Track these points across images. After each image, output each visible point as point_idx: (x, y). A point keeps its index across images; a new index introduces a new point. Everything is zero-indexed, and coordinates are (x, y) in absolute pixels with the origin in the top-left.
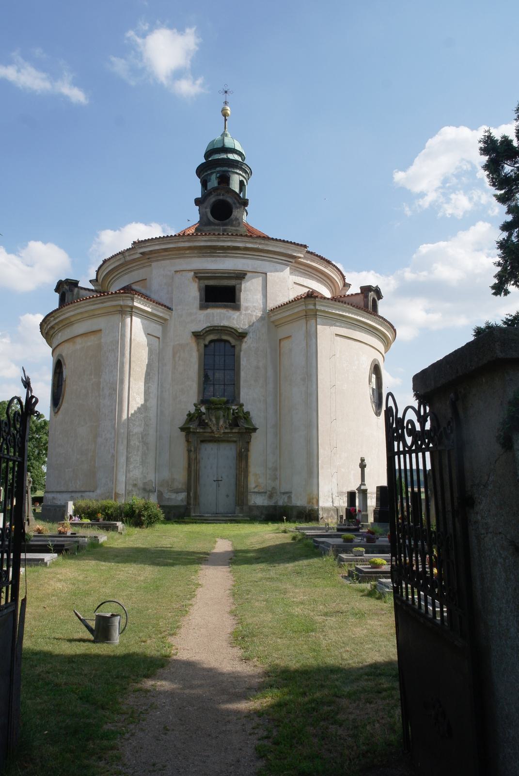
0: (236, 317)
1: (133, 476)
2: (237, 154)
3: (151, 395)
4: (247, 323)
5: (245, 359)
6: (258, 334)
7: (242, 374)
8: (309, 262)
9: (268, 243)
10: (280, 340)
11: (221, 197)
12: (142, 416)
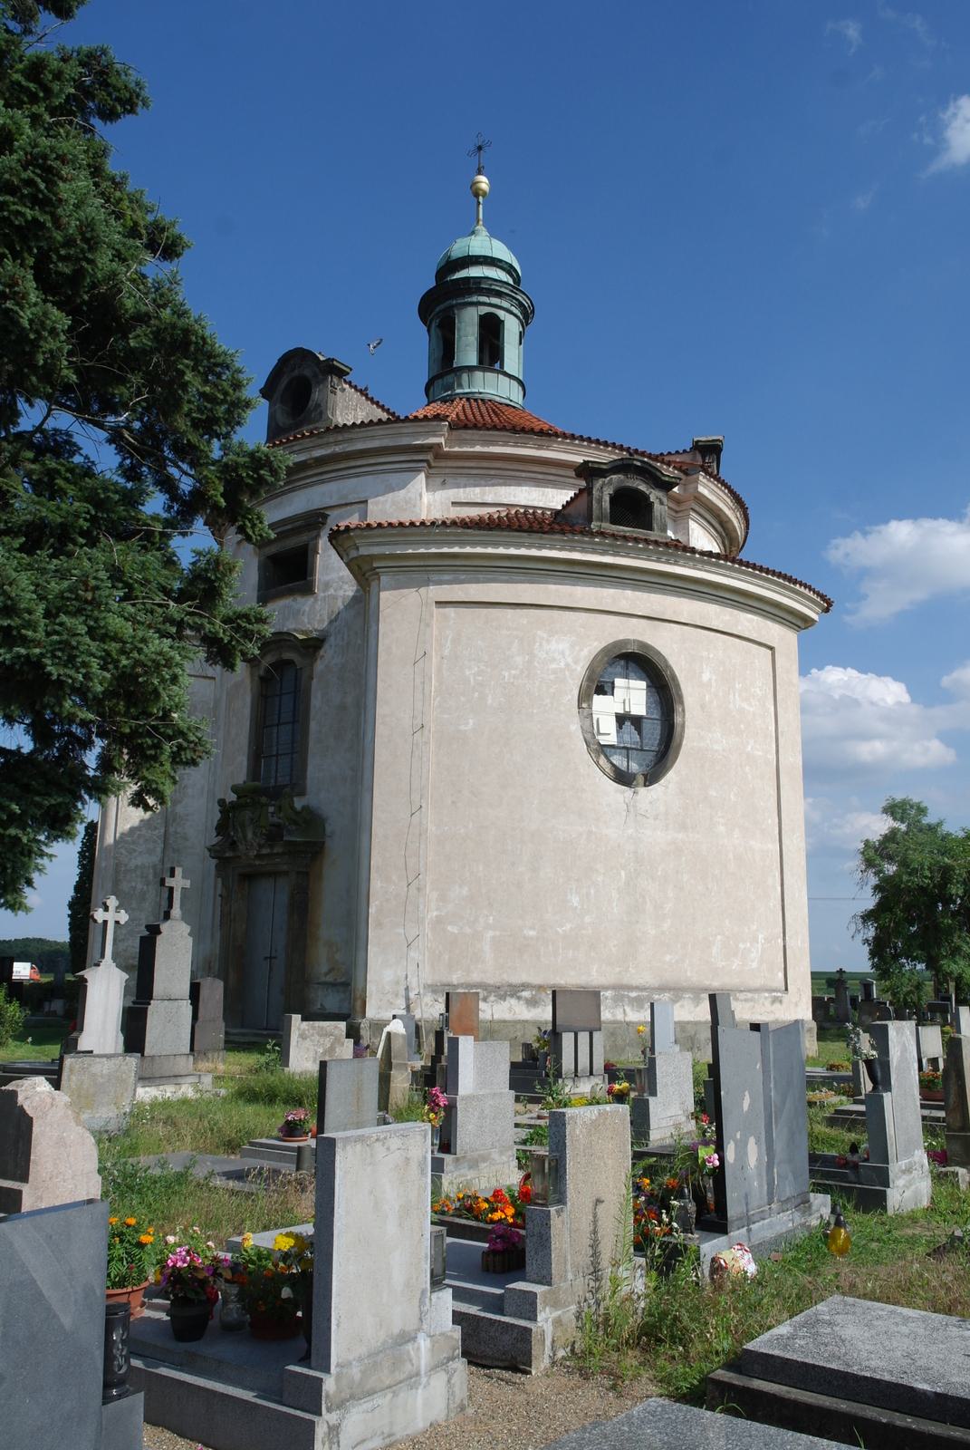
0: (307, 609)
1: (125, 951)
3: (190, 791)
4: (326, 618)
6: (345, 637)
7: (313, 726)
8: (478, 449)
10: (771, 648)
11: (296, 373)
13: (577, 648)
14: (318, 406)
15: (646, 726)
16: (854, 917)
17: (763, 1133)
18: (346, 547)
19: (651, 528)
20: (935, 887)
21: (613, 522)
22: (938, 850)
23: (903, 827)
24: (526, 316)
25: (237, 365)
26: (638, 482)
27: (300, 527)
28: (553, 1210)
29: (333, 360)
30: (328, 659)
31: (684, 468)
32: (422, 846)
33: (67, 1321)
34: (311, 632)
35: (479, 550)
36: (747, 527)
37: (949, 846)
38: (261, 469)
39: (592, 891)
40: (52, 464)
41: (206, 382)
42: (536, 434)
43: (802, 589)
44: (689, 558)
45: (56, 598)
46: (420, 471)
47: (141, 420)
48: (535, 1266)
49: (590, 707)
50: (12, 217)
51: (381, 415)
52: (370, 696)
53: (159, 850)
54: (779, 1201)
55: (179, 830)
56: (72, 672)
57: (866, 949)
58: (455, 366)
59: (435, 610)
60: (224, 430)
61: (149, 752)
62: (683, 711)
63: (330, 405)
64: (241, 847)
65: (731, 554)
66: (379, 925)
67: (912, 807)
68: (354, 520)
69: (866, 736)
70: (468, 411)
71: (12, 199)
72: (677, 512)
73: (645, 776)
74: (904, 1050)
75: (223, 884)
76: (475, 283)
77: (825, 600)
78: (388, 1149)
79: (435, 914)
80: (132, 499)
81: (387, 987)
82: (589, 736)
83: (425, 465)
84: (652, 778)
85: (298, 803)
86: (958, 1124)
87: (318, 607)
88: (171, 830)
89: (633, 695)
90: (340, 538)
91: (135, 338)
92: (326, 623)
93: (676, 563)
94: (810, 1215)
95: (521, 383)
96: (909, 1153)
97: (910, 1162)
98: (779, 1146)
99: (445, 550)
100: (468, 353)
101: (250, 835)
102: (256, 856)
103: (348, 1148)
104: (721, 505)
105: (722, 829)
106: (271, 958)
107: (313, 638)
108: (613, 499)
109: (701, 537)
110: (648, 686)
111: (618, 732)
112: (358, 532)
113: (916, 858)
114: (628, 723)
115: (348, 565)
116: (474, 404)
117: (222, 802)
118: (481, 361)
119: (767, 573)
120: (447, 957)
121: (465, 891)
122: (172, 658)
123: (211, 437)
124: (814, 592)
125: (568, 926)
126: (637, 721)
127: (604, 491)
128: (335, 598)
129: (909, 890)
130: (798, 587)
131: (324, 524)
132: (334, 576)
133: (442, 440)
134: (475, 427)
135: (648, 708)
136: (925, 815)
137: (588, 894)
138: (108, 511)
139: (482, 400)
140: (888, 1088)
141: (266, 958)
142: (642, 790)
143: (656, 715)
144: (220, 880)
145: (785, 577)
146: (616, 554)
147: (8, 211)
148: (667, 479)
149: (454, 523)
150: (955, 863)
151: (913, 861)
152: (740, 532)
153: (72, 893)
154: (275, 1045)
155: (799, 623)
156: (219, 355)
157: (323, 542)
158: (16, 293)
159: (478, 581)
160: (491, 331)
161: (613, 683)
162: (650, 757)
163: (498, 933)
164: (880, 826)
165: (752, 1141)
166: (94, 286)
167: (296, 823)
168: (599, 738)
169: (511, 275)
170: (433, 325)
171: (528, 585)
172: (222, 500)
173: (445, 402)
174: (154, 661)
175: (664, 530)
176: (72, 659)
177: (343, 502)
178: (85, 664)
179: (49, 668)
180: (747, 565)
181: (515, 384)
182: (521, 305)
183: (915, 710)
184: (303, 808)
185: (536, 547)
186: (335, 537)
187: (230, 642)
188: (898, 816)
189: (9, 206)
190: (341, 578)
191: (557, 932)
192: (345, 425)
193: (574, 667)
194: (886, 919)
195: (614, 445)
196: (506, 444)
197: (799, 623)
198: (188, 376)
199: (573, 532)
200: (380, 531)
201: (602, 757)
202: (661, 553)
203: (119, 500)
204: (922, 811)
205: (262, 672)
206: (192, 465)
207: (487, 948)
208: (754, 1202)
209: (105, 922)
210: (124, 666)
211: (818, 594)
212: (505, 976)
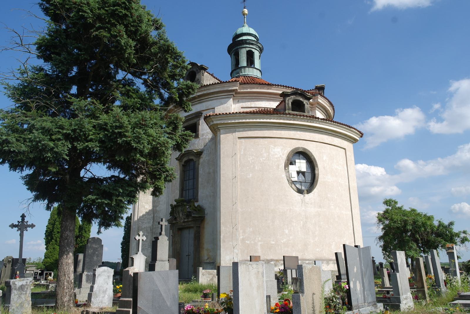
2: (246, 35)
3: (161, 203)
5: (202, 169)
7: (200, 180)
8: (249, 90)
9: (209, 88)
10: (345, 149)
12: (150, 216)
13: (283, 150)
14: (198, 80)
15: (306, 174)
16: (376, 238)
17: (361, 280)
18: (209, 121)
19: (304, 112)
20: (402, 227)
21: (292, 110)
22: (403, 215)
23: (390, 208)
24: (261, 50)
25: (183, 56)
26: (300, 98)
27: (194, 117)
28: (301, 295)
29: (203, 65)
30: (204, 158)
31: (314, 94)
32: (237, 215)
33: (168, 304)
34: (198, 150)
35: (251, 120)
36: (334, 113)
37: (406, 213)
38: (189, 89)
39: (292, 228)
40: (128, 88)
41: (174, 61)
42: (267, 85)
43: (353, 130)
44: (317, 121)
45: (134, 124)
46: (231, 98)
47: (152, 76)
48: (296, 313)
49: (288, 169)
50: (119, 13)
51: (217, 81)
52: (218, 168)
53: (151, 222)
54: (367, 303)
55: (158, 215)
56: (139, 145)
57: (381, 249)
58: (239, 66)
59: (238, 140)
60: (178, 78)
61: (158, 177)
62: (318, 169)
63: (202, 79)
64: (178, 219)
65: (329, 119)
66: (224, 241)
67: (393, 202)
68: (211, 113)
69: (373, 186)
70: (245, 80)
71: (119, 8)
72: (312, 108)
73: (307, 191)
74: (402, 260)
75: (173, 232)
76: (244, 41)
77: (361, 133)
78: (253, 267)
79: (242, 237)
80: (151, 99)
81: (227, 262)
82: (288, 178)
83: (232, 96)
84: (309, 191)
85: (196, 204)
86: (420, 286)
87: (200, 142)
88: (155, 215)
89: (302, 165)
90: (207, 119)
91: (153, 49)
92: (203, 147)
93: (313, 123)
94: (377, 309)
95: (260, 71)
96: (406, 293)
97: (406, 296)
98: (366, 285)
99: (240, 121)
100: (243, 62)
101: (181, 215)
102: (183, 222)
103: (242, 265)
104: (326, 105)
105: (332, 207)
106: (189, 255)
107: (199, 152)
108: (292, 103)
109: (319, 114)
110: (306, 162)
111: (298, 177)
112: (213, 116)
113: (395, 217)
114: (301, 174)
115: (210, 128)
116: (246, 78)
117: (171, 205)
118: (247, 65)
119: (342, 125)
120: (246, 251)
121: (251, 229)
122: (168, 142)
123: (174, 80)
124: (357, 131)
125: (285, 240)
126: (303, 173)
127: (289, 101)
128: (206, 139)
129: (394, 228)
130: (352, 129)
131: (201, 116)
132: (205, 132)
133: (237, 88)
134: (248, 83)
135: (307, 169)
136: (397, 204)
137: (291, 229)
138: (145, 102)
139: (249, 76)
140: (398, 271)
141: (187, 256)
142: (306, 195)
143: (309, 171)
144: (171, 231)
145: (348, 126)
146: (294, 120)
147: (118, 11)
148: (309, 96)
149: (243, 113)
150: (408, 219)
151: (394, 218)
152: (332, 114)
153: (122, 240)
154: (194, 278)
155: (353, 141)
156: (178, 53)
157: (202, 121)
158: (120, 35)
159: (251, 130)
160: (250, 55)
161: (295, 161)
162: (308, 184)
163: (262, 243)
164: (383, 208)
165: (358, 282)
166: (140, 34)
167: (195, 211)
168: (292, 179)
169: (256, 38)
170: (232, 54)
171: (267, 131)
172: (178, 99)
173: (237, 78)
174: (163, 142)
175: (309, 112)
176: (139, 141)
177: (207, 109)
178: (143, 143)
179: (133, 144)
180: (336, 122)
181: (258, 71)
182: (259, 47)
183: (388, 176)
184: (198, 205)
185: (269, 119)
186: (206, 118)
187: (181, 143)
188: (388, 205)
189: (118, 10)
190: (207, 132)
191: (281, 242)
192: (207, 85)
193: (283, 156)
194: (387, 238)
195: (291, 87)
196: (257, 88)
197: (353, 141)
198: (169, 60)
199: (280, 114)
200: (220, 116)
201: (293, 185)
202: (308, 119)
203: (148, 98)
204: (396, 203)
205: (183, 163)
206: (168, 90)
207: (259, 248)
208: (360, 302)
209: (139, 240)
210: (154, 145)
211: (359, 131)
212: (265, 257)
